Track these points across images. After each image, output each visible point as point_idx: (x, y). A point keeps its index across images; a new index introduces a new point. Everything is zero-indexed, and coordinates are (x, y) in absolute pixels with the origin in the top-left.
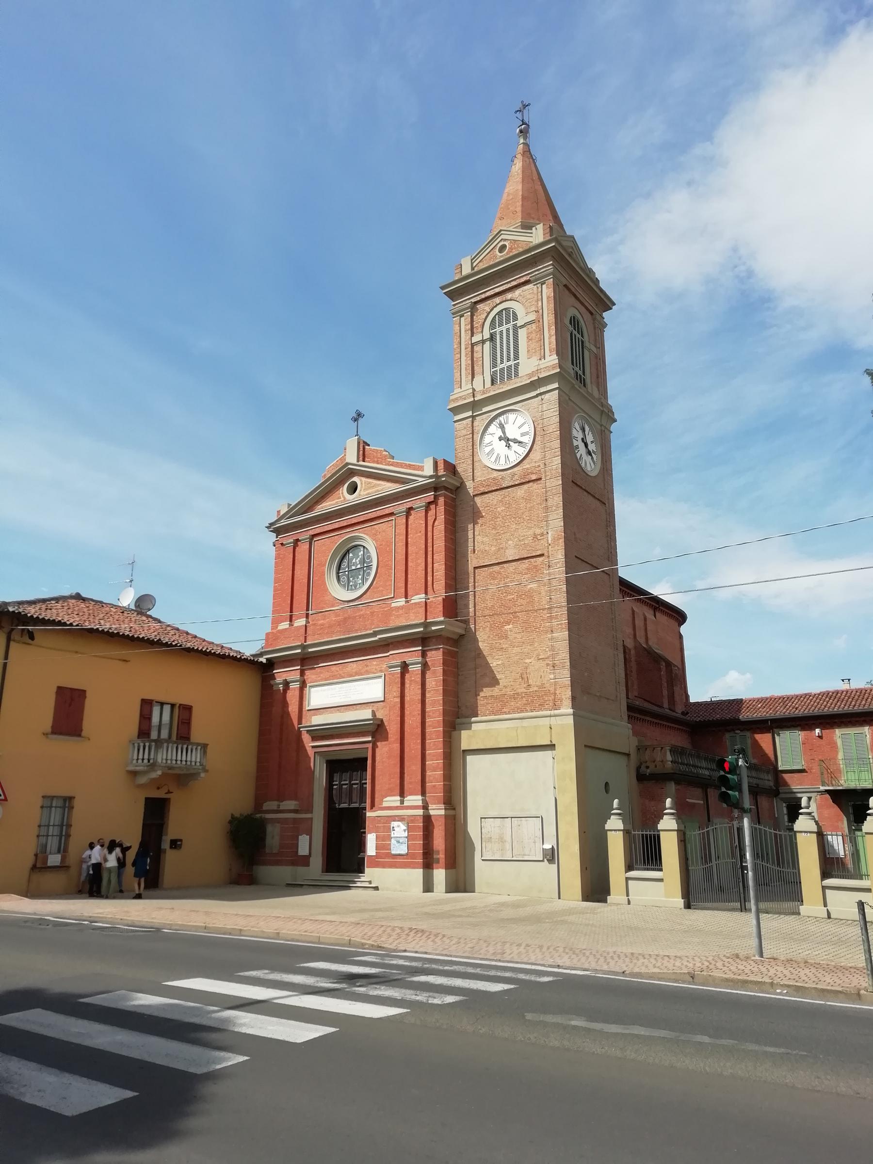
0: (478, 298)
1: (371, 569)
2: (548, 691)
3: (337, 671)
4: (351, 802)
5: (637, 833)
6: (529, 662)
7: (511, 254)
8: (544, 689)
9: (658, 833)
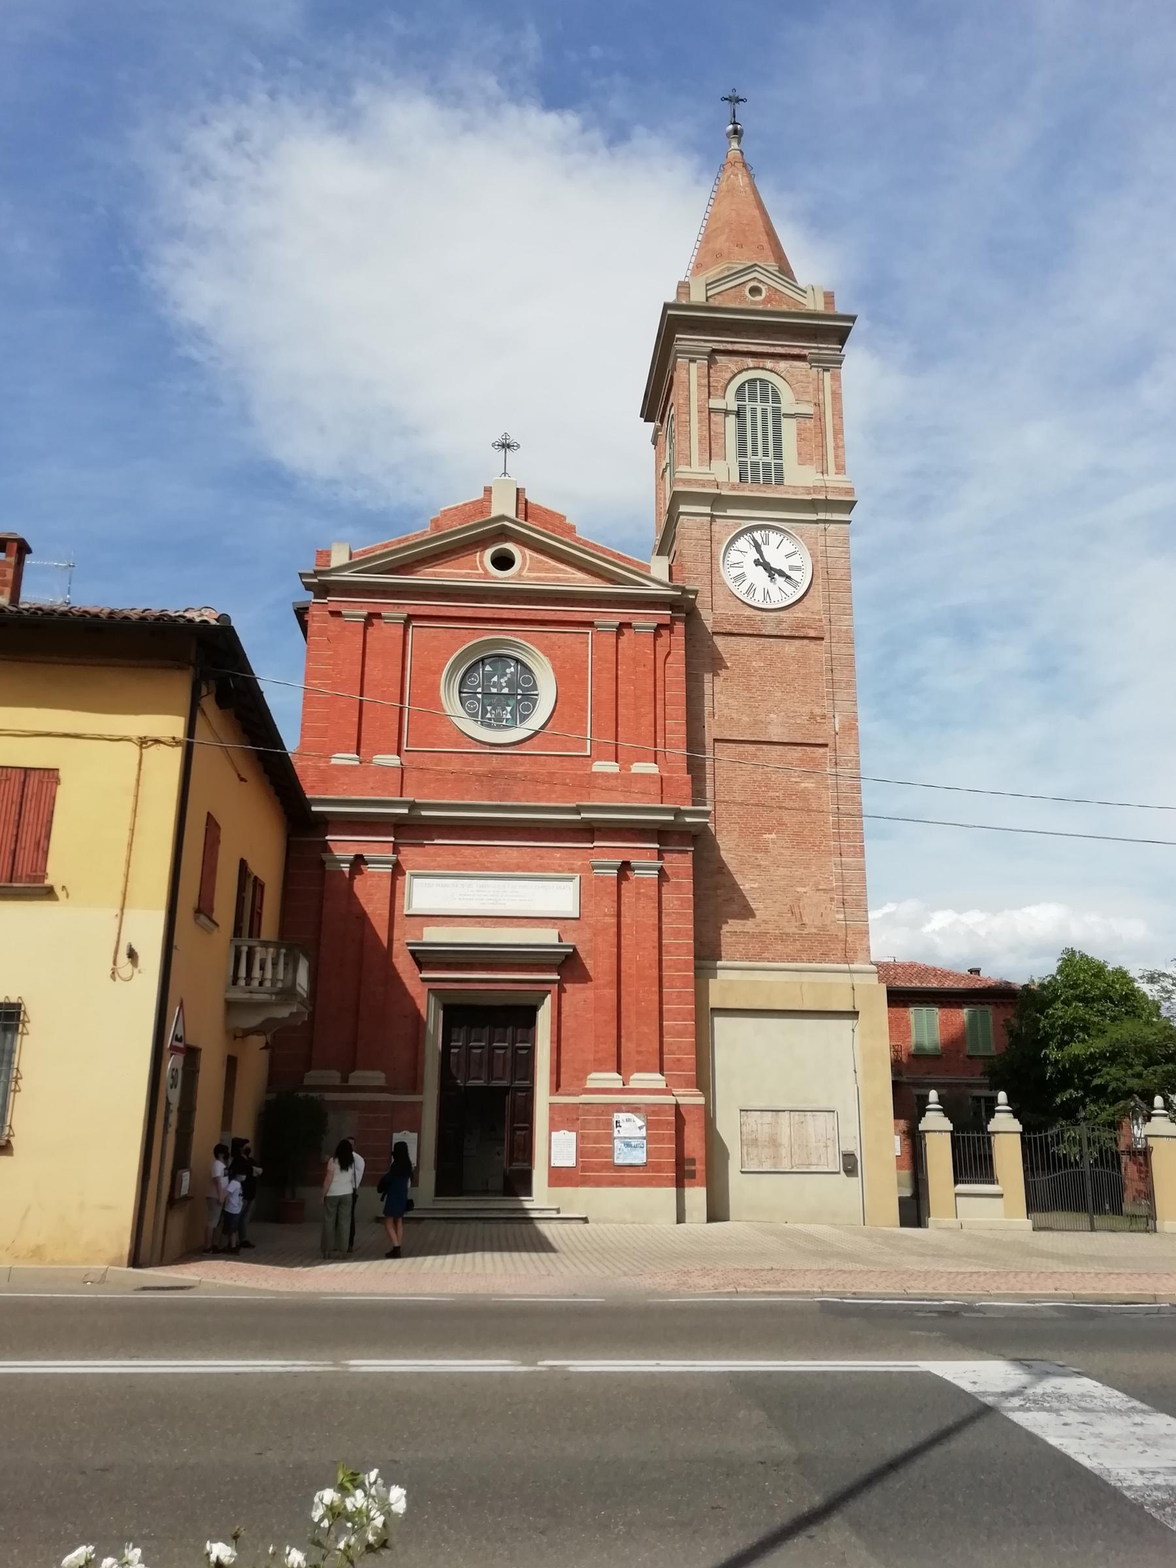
0: (721, 347)
3: (475, 857)
4: (491, 1077)
5: (960, 1134)
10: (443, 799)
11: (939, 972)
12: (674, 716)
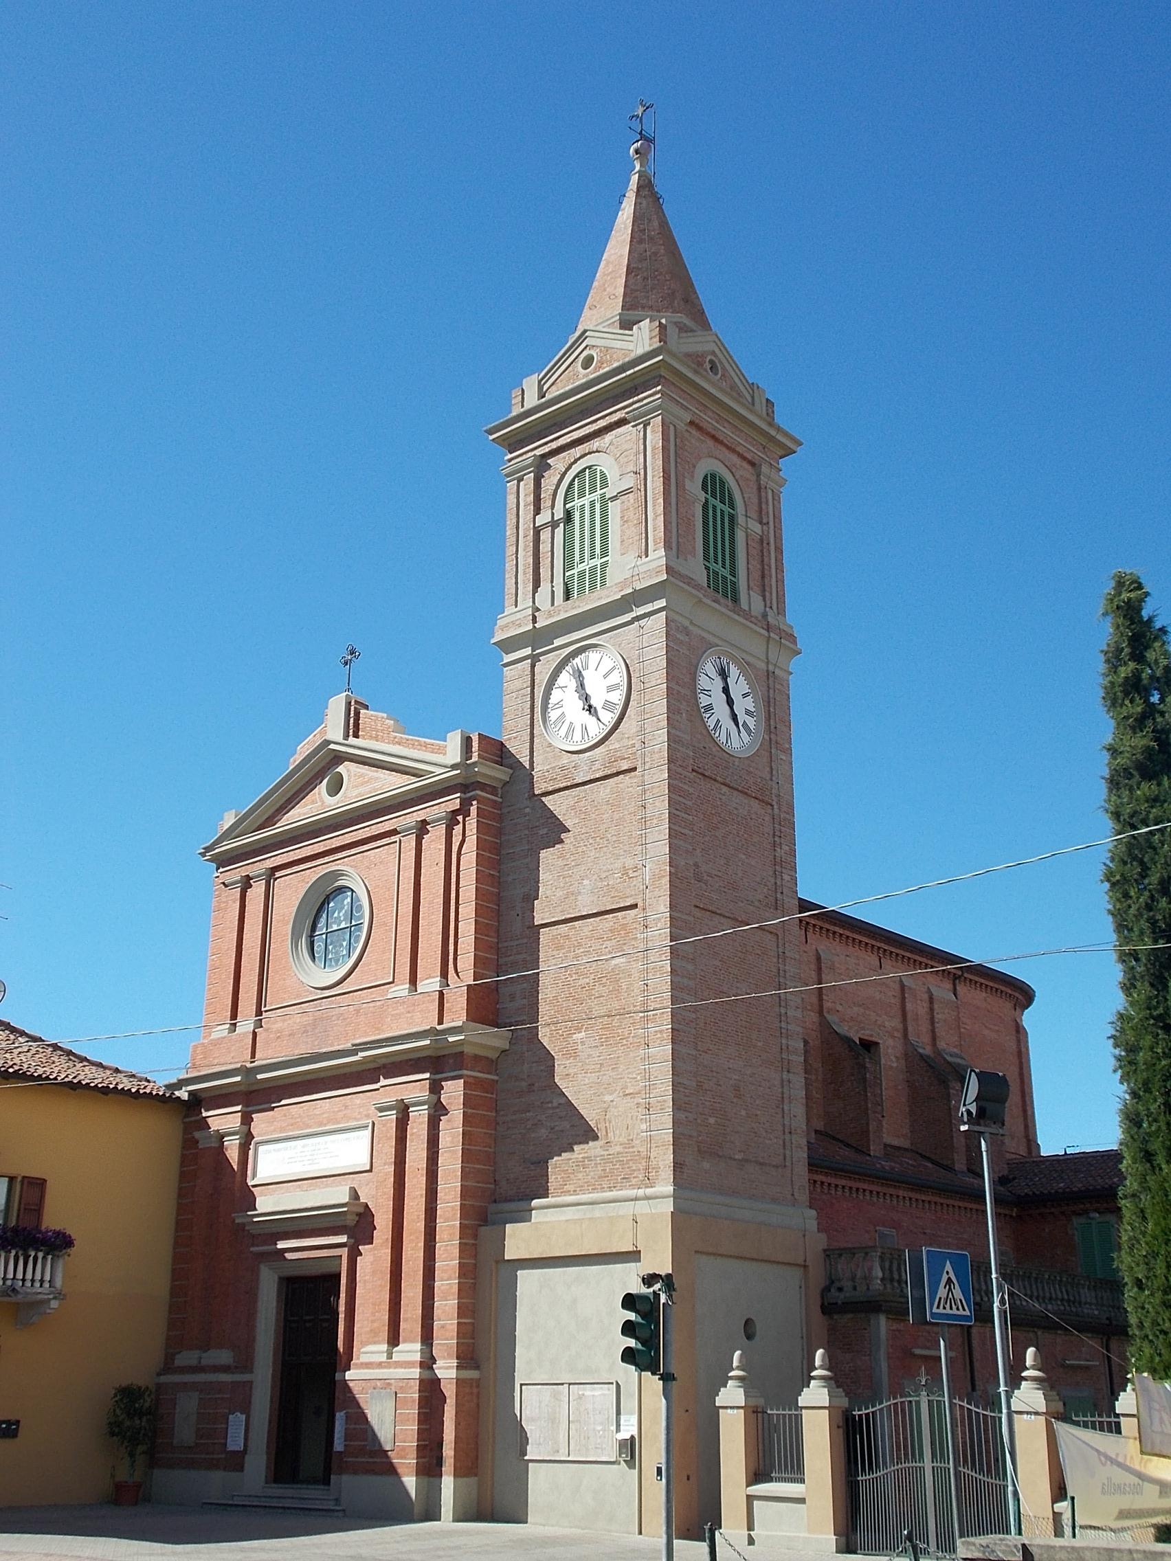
0: (546, 449)
1: (360, 930)
7: (602, 371)
8: (631, 1150)
9: (1116, 1420)
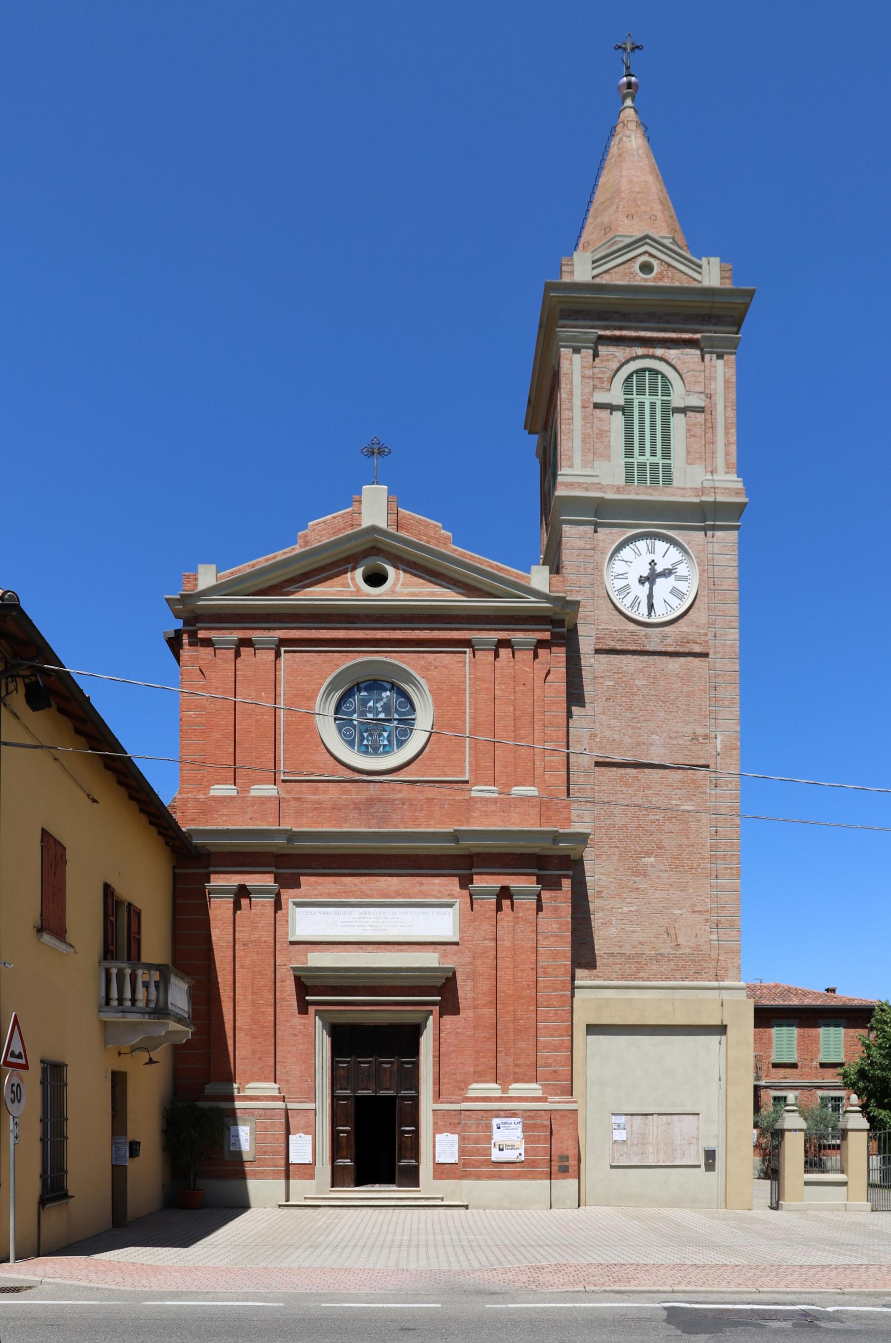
2: (707, 955)
3: (356, 885)
6: (678, 913)
10: (322, 827)
11: (800, 992)
12: (555, 738)
